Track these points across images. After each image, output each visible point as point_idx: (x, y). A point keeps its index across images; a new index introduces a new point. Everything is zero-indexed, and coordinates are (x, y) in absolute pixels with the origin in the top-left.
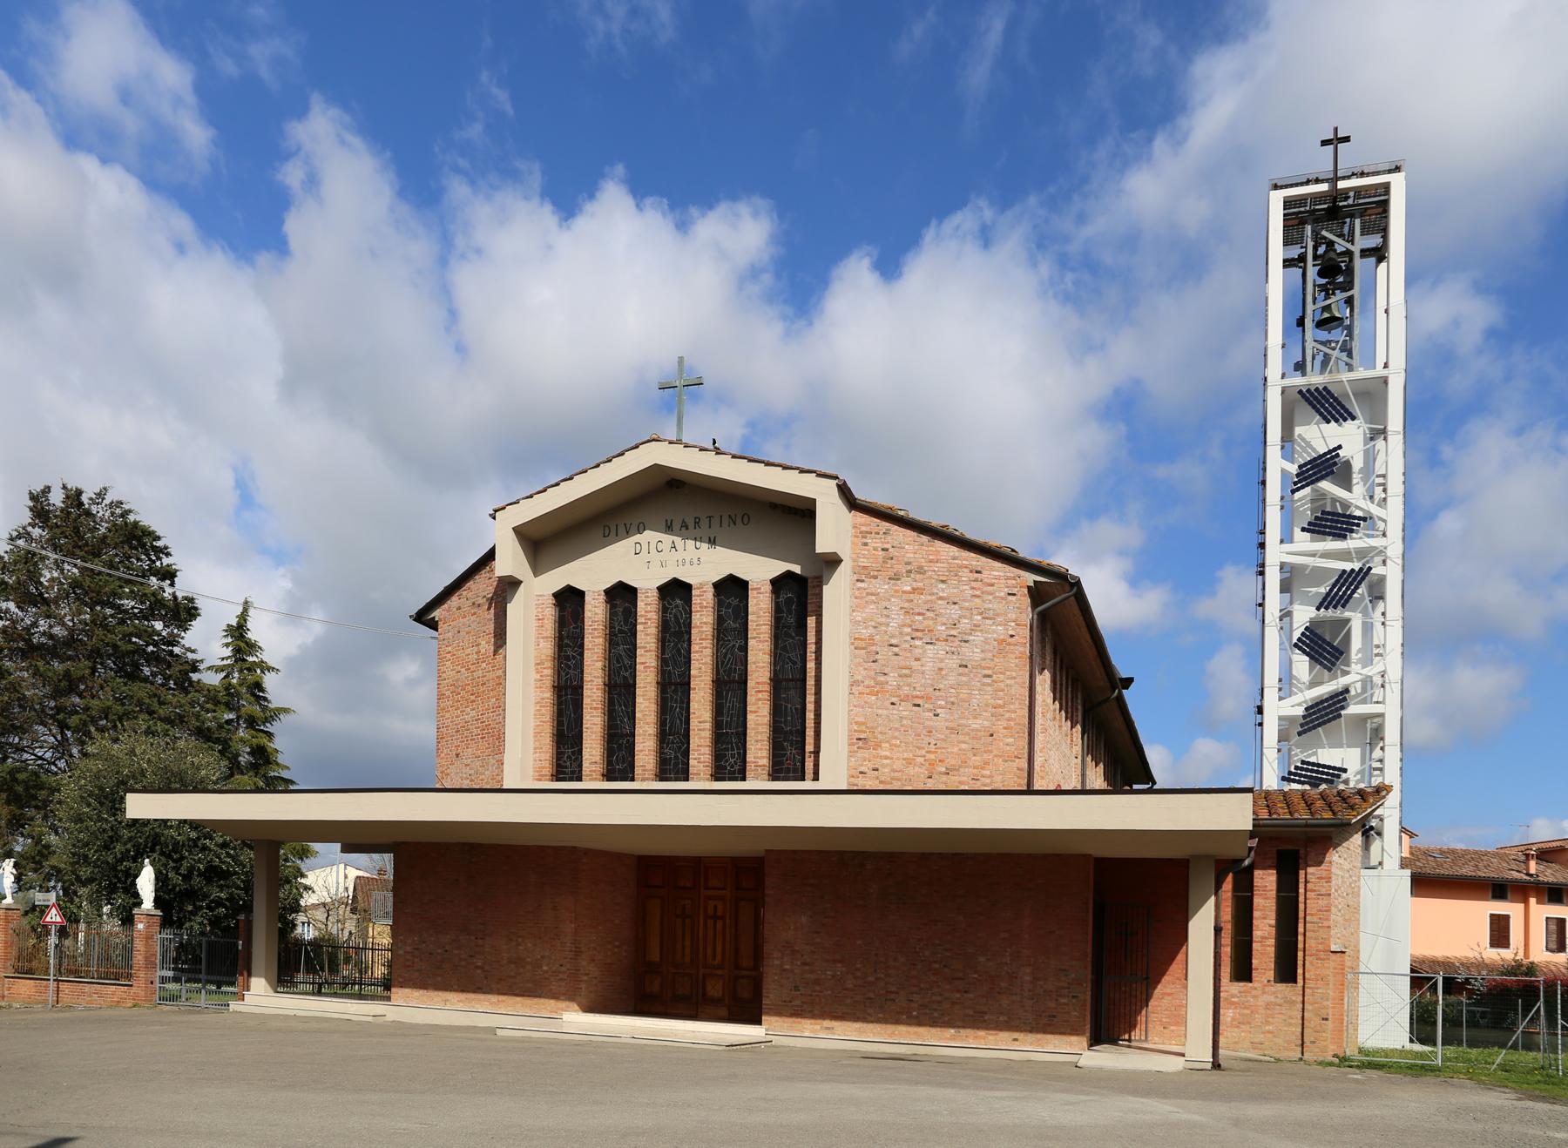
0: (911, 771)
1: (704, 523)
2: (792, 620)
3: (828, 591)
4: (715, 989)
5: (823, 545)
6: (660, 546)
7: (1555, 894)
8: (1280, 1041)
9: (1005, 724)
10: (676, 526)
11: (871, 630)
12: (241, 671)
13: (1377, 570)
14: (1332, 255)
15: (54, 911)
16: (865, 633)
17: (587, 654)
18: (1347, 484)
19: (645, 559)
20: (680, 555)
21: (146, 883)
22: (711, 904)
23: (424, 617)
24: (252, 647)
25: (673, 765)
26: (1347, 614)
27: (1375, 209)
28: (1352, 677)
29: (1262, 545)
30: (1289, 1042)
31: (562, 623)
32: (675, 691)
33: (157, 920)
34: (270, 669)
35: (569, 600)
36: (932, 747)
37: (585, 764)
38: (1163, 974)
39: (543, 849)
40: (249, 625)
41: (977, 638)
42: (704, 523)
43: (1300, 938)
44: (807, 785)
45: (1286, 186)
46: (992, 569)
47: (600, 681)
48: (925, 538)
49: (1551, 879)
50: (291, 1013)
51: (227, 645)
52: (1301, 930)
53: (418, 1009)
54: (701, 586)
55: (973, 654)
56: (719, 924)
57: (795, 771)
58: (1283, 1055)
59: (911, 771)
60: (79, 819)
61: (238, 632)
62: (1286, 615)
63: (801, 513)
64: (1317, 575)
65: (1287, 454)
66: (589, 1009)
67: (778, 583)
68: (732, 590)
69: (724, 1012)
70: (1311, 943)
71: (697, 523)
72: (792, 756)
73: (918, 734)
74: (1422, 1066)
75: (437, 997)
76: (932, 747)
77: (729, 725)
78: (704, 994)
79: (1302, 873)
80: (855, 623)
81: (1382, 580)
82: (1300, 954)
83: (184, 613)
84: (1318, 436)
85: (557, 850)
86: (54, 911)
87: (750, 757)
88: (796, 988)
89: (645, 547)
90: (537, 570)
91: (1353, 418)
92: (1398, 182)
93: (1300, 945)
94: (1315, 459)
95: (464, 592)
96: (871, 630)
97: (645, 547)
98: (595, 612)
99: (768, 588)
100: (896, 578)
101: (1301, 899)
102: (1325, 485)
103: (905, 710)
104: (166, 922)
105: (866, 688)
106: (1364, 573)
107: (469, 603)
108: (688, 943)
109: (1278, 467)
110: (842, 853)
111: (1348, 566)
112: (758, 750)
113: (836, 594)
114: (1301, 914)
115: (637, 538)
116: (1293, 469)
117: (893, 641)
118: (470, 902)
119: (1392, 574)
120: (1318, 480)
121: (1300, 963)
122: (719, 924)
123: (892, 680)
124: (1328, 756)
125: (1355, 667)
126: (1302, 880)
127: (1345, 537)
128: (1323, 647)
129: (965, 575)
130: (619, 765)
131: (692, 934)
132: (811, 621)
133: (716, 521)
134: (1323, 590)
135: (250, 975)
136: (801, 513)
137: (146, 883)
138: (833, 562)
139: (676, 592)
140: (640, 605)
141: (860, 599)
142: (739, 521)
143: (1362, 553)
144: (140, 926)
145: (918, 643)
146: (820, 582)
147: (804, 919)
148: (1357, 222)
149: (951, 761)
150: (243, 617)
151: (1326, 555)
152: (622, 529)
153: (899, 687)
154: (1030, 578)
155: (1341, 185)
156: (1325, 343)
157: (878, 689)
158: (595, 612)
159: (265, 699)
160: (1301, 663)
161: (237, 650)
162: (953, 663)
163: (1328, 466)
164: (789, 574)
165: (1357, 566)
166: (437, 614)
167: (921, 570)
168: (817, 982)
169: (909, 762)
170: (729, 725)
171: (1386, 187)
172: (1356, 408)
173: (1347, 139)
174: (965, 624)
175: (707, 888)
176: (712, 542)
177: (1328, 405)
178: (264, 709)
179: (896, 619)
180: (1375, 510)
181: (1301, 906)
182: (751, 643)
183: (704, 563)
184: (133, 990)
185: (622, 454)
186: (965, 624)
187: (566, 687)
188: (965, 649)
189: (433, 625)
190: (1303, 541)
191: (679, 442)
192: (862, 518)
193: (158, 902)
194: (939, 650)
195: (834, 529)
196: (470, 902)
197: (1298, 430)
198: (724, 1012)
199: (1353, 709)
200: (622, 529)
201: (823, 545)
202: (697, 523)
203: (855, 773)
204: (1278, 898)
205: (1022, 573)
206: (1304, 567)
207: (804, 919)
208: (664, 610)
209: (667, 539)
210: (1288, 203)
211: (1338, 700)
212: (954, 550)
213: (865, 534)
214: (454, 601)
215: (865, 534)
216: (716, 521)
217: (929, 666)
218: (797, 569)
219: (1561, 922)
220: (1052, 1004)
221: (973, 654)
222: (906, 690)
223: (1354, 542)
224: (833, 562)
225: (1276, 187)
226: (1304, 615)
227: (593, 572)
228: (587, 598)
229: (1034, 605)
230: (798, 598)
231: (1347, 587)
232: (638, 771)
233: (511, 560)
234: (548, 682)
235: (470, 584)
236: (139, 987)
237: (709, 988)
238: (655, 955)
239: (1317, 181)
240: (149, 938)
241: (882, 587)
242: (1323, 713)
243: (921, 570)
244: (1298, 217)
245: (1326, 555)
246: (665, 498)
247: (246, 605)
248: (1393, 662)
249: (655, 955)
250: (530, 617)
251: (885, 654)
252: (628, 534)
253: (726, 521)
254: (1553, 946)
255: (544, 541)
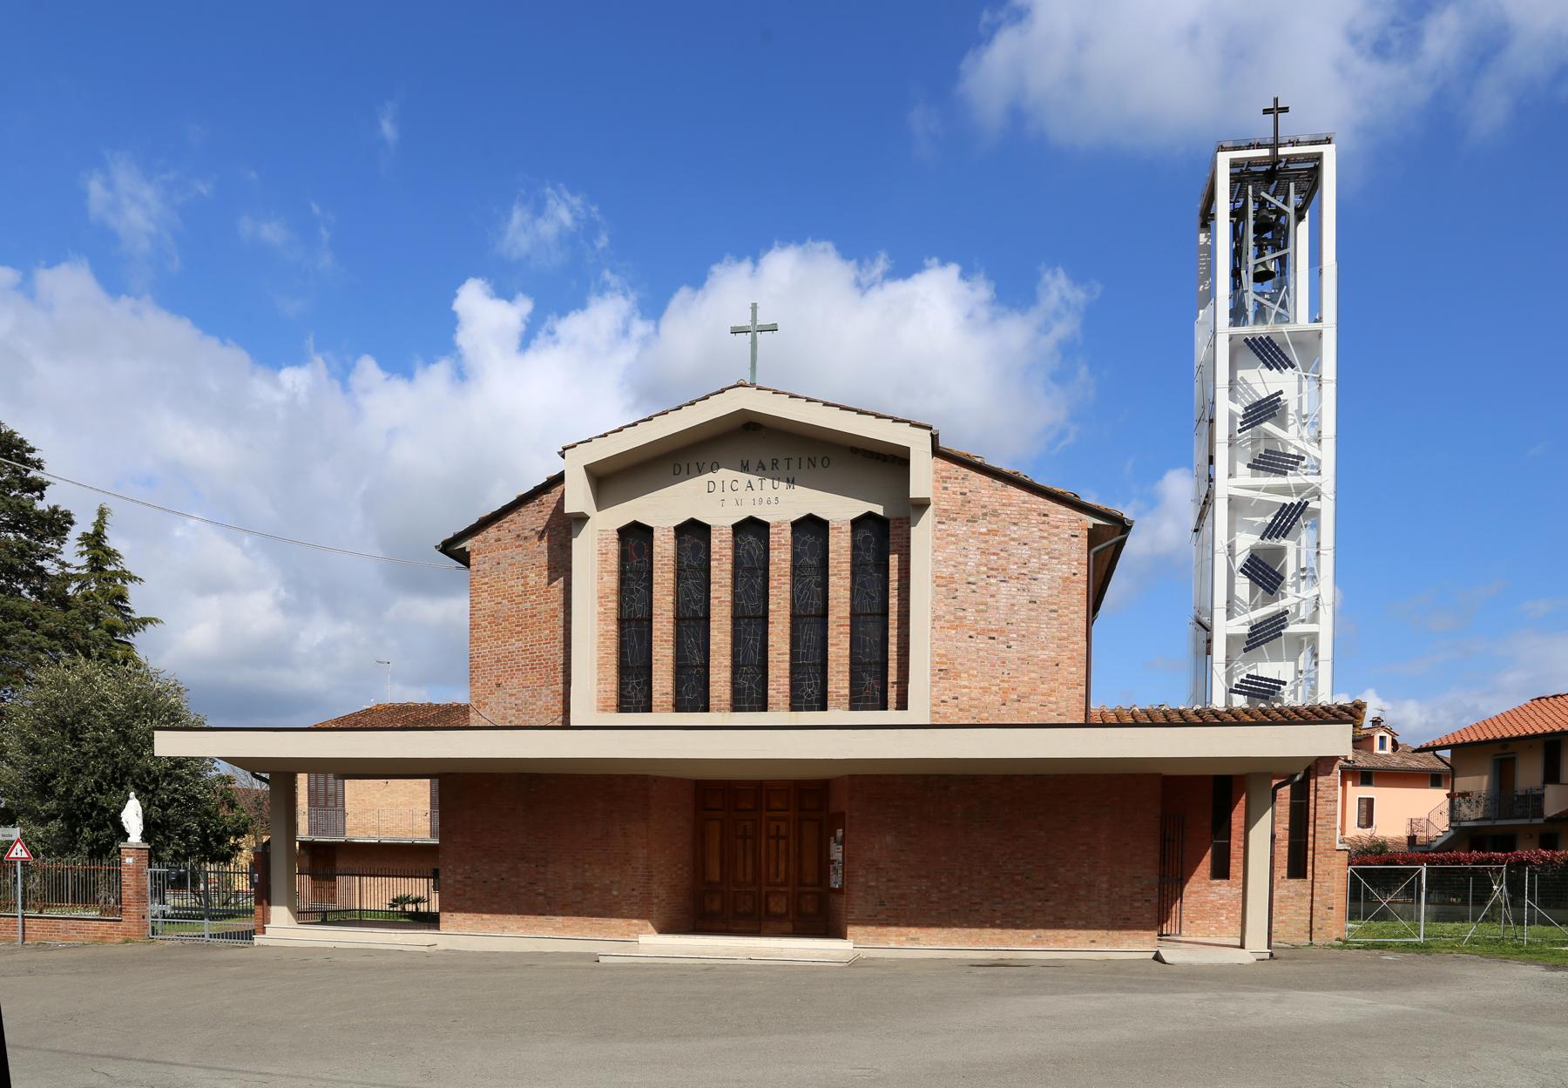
0: (987, 699)
1: (782, 464)
2: (870, 558)
3: (915, 532)
4: (778, 905)
5: (916, 491)
6: (735, 486)
7: (8, 614)
8: (1291, 929)
9: (1068, 654)
10: (753, 464)
11: (951, 569)
12: (98, 581)
13: (1313, 505)
14: (1265, 213)
15: (19, 846)
16: (946, 571)
17: (656, 588)
18: (1283, 425)
19: (720, 498)
20: (757, 494)
21: (132, 816)
22: (773, 825)
23: (454, 548)
24: (112, 555)
25: (751, 695)
26: (1283, 542)
27: (1311, 176)
28: (1290, 598)
29: (1211, 480)
30: (1299, 930)
31: (624, 557)
32: (749, 624)
33: (146, 853)
34: (132, 578)
35: (636, 537)
36: (1006, 677)
37: (655, 695)
38: (1191, 875)
39: (609, 777)
40: (106, 532)
41: (1044, 576)
42: (782, 464)
43: (1310, 839)
44: (891, 716)
45: (1235, 149)
46: (1057, 512)
47: (671, 614)
48: (998, 484)
49: (1364, 765)
50: (331, 945)
51: (82, 554)
52: (1311, 832)
53: (469, 936)
54: (779, 524)
55: (1041, 590)
56: (782, 843)
57: (874, 700)
58: (1296, 941)
59: (987, 699)
60: (35, 749)
61: (95, 541)
62: (1231, 547)
63: (895, 460)
64: (1261, 507)
65: (1233, 398)
66: (663, 930)
67: (856, 523)
68: (811, 529)
69: (788, 926)
70: (1320, 844)
71: (774, 464)
72: (877, 683)
73: (989, 668)
74: (1408, 945)
75: (512, 922)
76: (1006, 677)
77: (805, 656)
78: (767, 910)
79: (1312, 782)
80: (937, 562)
81: (1317, 512)
82: (1310, 853)
83: (57, 524)
84: (1263, 381)
85: (627, 779)
86: (19, 846)
87: (831, 688)
88: (882, 903)
89: (719, 485)
90: (600, 505)
91: (1293, 366)
92: (1329, 153)
93: (1310, 845)
94: (1255, 404)
95: (505, 523)
96: (951, 569)
97: (719, 485)
98: (664, 548)
99: (849, 528)
100: (973, 520)
101: (1312, 805)
102: (1267, 426)
103: (981, 642)
104: (153, 856)
105: (949, 623)
106: (1301, 508)
107: (513, 535)
108: (749, 862)
109: (1227, 409)
110: (926, 777)
111: (1288, 500)
112: (839, 681)
113: (922, 534)
114: (1311, 819)
115: (710, 476)
116: (1239, 410)
117: (971, 579)
118: (515, 833)
119: (1326, 507)
120: (1261, 422)
121: (1310, 860)
122: (782, 843)
123: (970, 615)
124: (1267, 669)
125: (1290, 590)
126: (1312, 789)
127: (1285, 474)
128: (1264, 573)
129: (1034, 517)
130: (691, 694)
131: (757, 854)
132: (894, 560)
133: (795, 463)
134: (1269, 519)
135: (269, 904)
136: (895, 460)
137: (132, 816)
138: (922, 505)
139: (752, 530)
140: (714, 542)
141: (941, 540)
142: (818, 464)
143: (1299, 489)
144: (129, 860)
145: (993, 581)
146: (906, 523)
147: (888, 839)
148: (1292, 185)
149: (1022, 689)
150: (100, 525)
151: (1268, 490)
152: (693, 468)
153: (976, 621)
154: (1091, 521)
155: (1282, 151)
156: (1261, 294)
157: (957, 624)
158: (664, 548)
159: (128, 609)
160: (1243, 585)
161: (94, 559)
162: (1023, 599)
163: (1267, 409)
164: (870, 516)
165: (1296, 500)
166: (468, 544)
167: (995, 513)
168: (902, 896)
169: (985, 690)
170: (805, 656)
171: (1318, 157)
172: (1294, 355)
173: (1286, 110)
174: (1034, 563)
175: (768, 810)
176: (791, 481)
177: (1269, 353)
178: (126, 619)
179: (974, 558)
180: (1312, 449)
181: (1312, 812)
182: (832, 579)
183: (782, 503)
184: (121, 926)
185: (706, 398)
186: (1034, 563)
187: (629, 620)
188: (1034, 587)
189: (463, 558)
190: (1244, 475)
191: (753, 385)
192: (943, 464)
193: (146, 836)
194: (1012, 587)
195: (924, 476)
196: (515, 833)
197: (1240, 373)
198: (788, 926)
199: (1292, 628)
200: (693, 468)
201: (916, 491)
202: (774, 464)
203: (936, 701)
204: (1292, 805)
205: (1083, 516)
206: (1250, 500)
207: (888, 839)
208: (736, 546)
209: (744, 478)
210: (1234, 164)
211: (1279, 620)
212: (1024, 495)
213: (945, 479)
214: (492, 532)
215: (945, 479)
216: (795, 463)
217: (1003, 602)
218: (879, 510)
219: (1370, 802)
220: (1127, 908)
221: (1041, 590)
222: (982, 624)
223: (1291, 479)
224: (922, 505)
225: (1223, 149)
226: (1247, 541)
227: (663, 509)
228: (655, 534)
229: (1090, 546)
230: (882, 539)
231: (1288, 519)
232: (713, 701)
233: (577, 496)
234: (613, 615)
235: (514, 516)
236: (129, 922)
237: (772, 904)
238: (714, 873)
239: (1259, 146)
240: (139, 872)
241: (961, 529)
242: (1265, 634)
243: (995, 513)
244: (1242, 176)
245: (1268, 490)
246: (750, 440)
247: (102, 513)
248: (1326, 586)
249: (714, 873)
250: (593, 555)
251: (963, 591)
252: (700, 472)
253: (805, 462)
254: (1363, 823)
255: (610, 479)
